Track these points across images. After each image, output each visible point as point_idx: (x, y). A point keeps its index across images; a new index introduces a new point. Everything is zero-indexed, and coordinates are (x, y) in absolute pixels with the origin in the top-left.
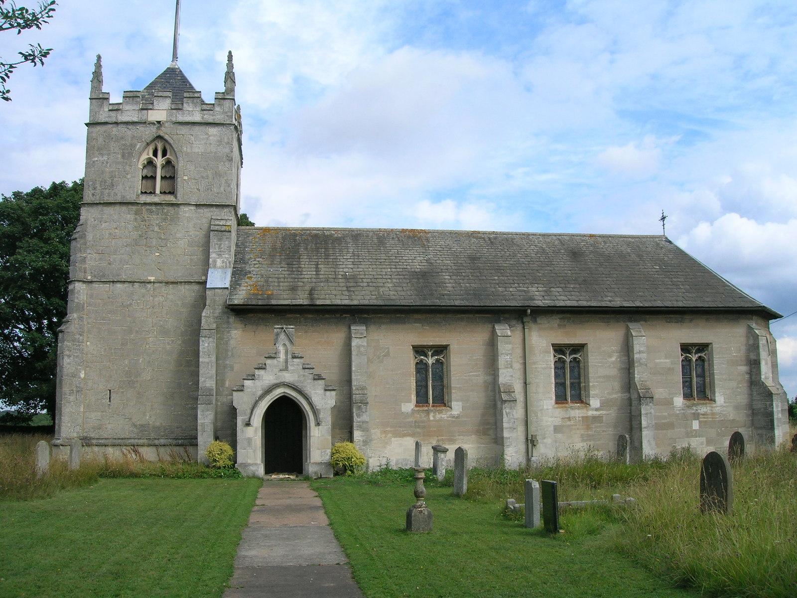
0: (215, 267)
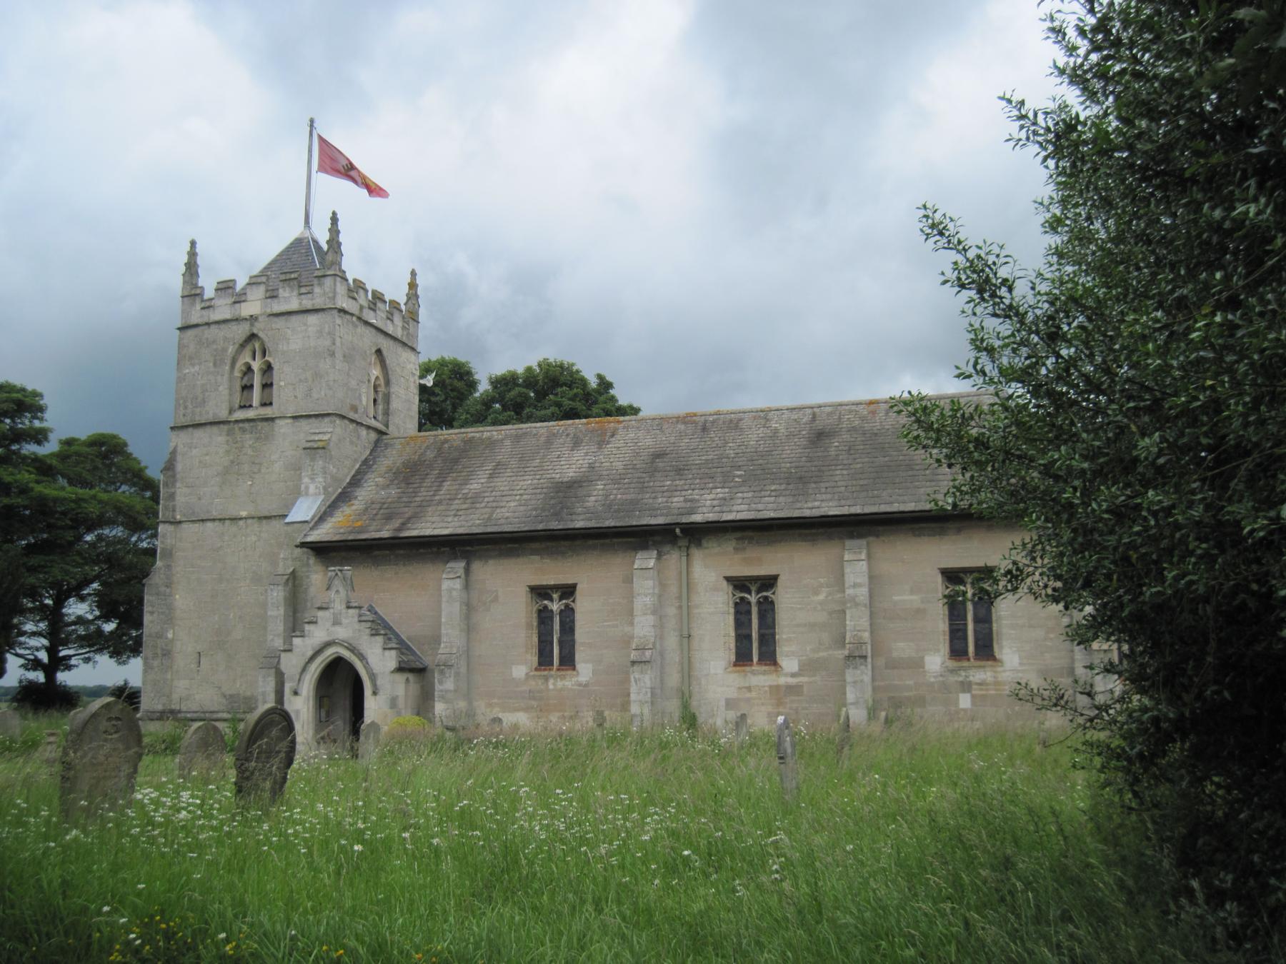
0: (307, 494)
